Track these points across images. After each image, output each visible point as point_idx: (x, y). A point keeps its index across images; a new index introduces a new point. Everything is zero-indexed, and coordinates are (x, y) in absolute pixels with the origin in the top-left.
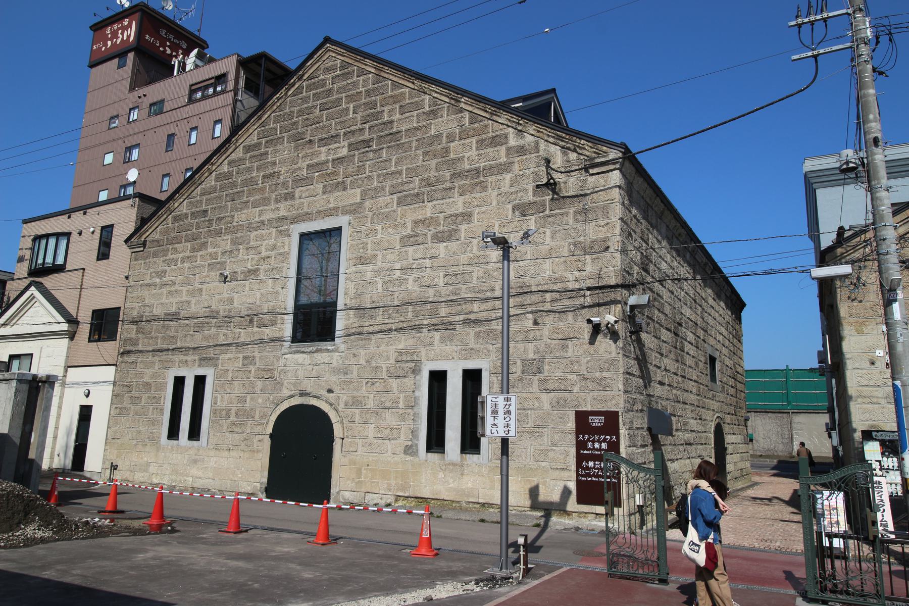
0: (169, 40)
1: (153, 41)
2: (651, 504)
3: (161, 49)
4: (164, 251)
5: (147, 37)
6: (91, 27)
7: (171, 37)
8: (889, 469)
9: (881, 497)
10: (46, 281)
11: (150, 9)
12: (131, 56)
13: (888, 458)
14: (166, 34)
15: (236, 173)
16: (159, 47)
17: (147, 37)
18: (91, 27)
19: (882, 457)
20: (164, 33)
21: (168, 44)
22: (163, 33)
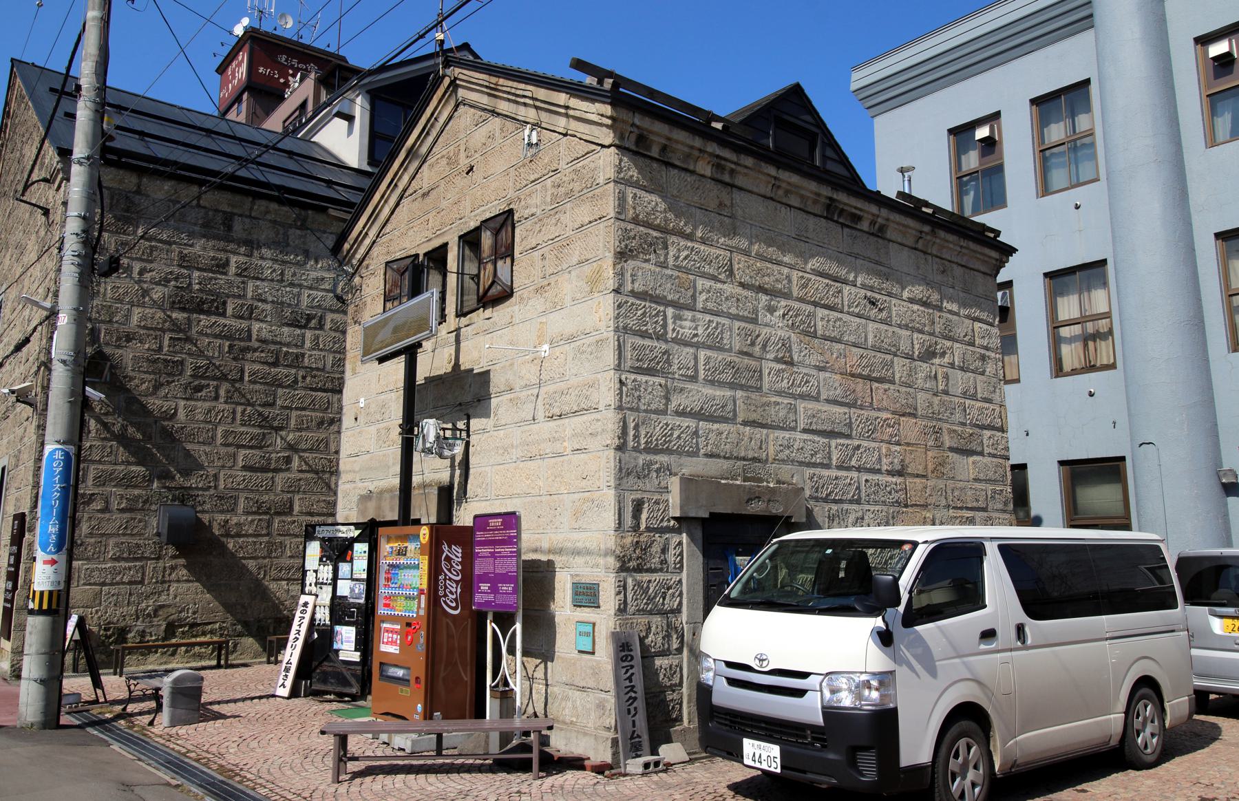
0: (292, 67)
1: (270, 72)
2: (91, 535)
3: (282, 81)
4: (312, 307)
5: (261, 70)
6: (217, 71)
7: (295, 62)
8: (322, 583)
9: (631, 681)
10: (45, 313)
11: (261, 34)
12: (245, 96)
13: (324, 566)
14: (286, 60)
15: (692, 240)
16: (279, 78)
17: (261, 70)
18: (217, 71)
19: (320, 565)
20: (284, 59)
21: (291, 72)
22: (283, 59)
